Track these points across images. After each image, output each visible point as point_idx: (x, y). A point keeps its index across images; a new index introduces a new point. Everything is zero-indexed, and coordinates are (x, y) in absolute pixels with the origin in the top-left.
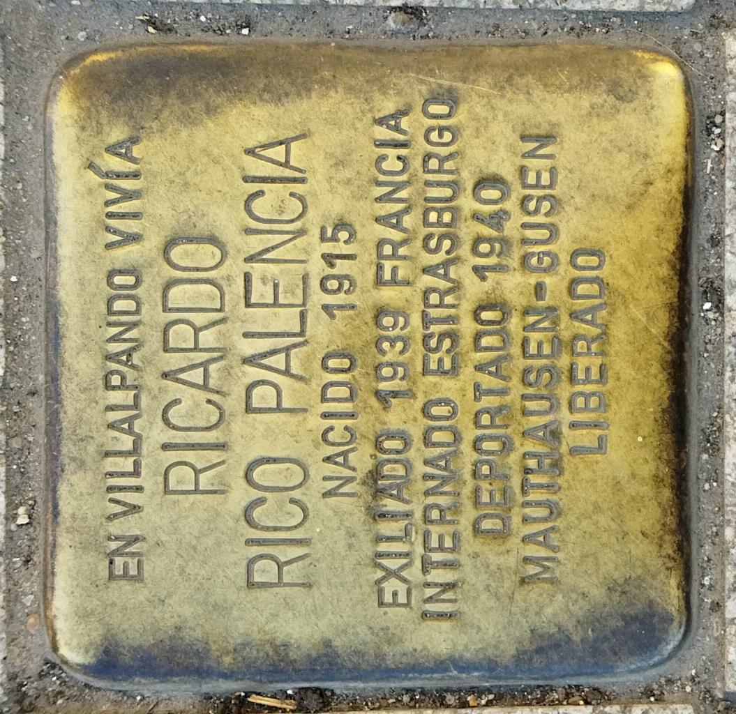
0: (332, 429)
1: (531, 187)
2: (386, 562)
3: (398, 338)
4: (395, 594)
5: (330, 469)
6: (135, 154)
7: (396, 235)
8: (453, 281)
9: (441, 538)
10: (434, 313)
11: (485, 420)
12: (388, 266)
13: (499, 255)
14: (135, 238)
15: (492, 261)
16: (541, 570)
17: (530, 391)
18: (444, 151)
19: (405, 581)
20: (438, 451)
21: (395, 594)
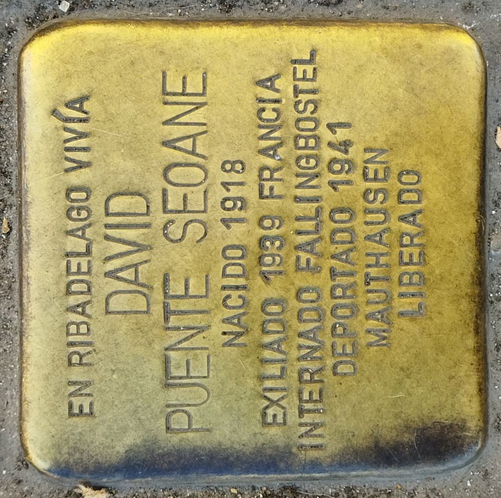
0: (228, 297)
3: (276, 238)
4: (275, 416)
6: (277, 87)
11: (339, 292)
12: (267, 185)
13: (347, 172)
14: (81, 165)
15: (342, 177)
19: (283, 408)
21: (275, 416)
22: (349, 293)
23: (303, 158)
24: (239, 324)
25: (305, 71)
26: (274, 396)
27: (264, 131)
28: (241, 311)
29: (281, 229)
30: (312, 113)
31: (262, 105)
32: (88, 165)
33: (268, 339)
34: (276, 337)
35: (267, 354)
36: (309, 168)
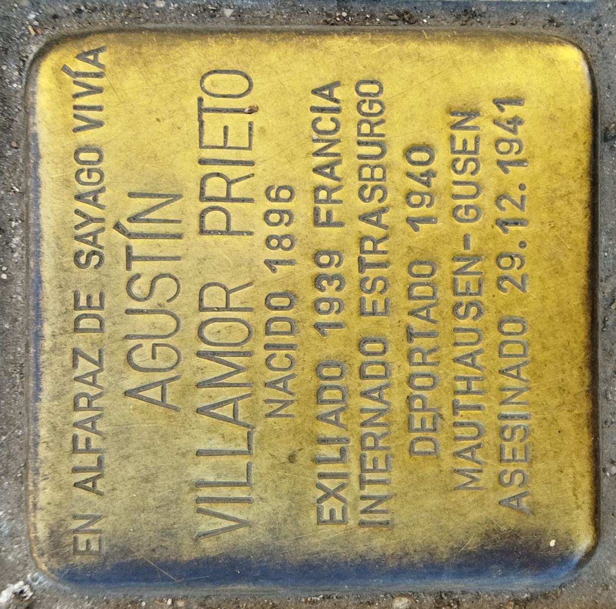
1: (459, 152)
2: (326, 482)
4: (332, 512)
5: (271, 394)
8: (386, 227)
9: (375, 461)
10: (369, 258)
11: (417, 357)
18: (374, 119)
21: (332, 512)
22: (429, 359)
28: (287, 373)
31: (317, 115)
32: (99, 124)
33: (325, 409)
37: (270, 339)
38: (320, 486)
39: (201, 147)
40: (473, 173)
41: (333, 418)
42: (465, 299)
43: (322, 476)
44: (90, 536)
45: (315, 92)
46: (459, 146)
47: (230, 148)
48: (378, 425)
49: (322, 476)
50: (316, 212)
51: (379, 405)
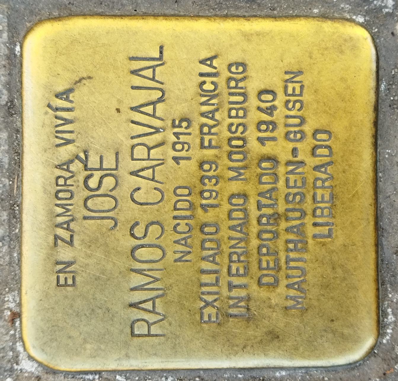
0: (178, 224)
1: (289, 95)
3: (214, 177)
7: (211, 122)
11: (264, 220)
12: (207, 138)
14: (68, 142)
16: (65, 210)
17: (291, 206)
20: (235, 222)
21: (209, 316)
23: (233, 66)
24: (186, 245)
25: (66, 279)
26: (210, 298)
27: (204, 99)
29: (217, 186)
30: (242, 133)
34: (211, 252)
35: (206, 266)
36: (238, 73)
37: (176, 213)
38: (201, 299)
39: (133, 159)
40: (299, 110)
41: (211, 259)
42: (295, 191)
43: (203, 293)
44: (66, 275)
45: (202, 62)
46: (290, 91)
47: (153, 336)
48: (239, 248)
49: (203, 293)
50: (202, 140)
51: (239, 235)
